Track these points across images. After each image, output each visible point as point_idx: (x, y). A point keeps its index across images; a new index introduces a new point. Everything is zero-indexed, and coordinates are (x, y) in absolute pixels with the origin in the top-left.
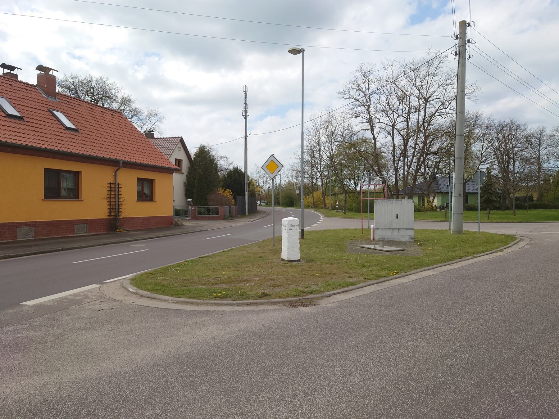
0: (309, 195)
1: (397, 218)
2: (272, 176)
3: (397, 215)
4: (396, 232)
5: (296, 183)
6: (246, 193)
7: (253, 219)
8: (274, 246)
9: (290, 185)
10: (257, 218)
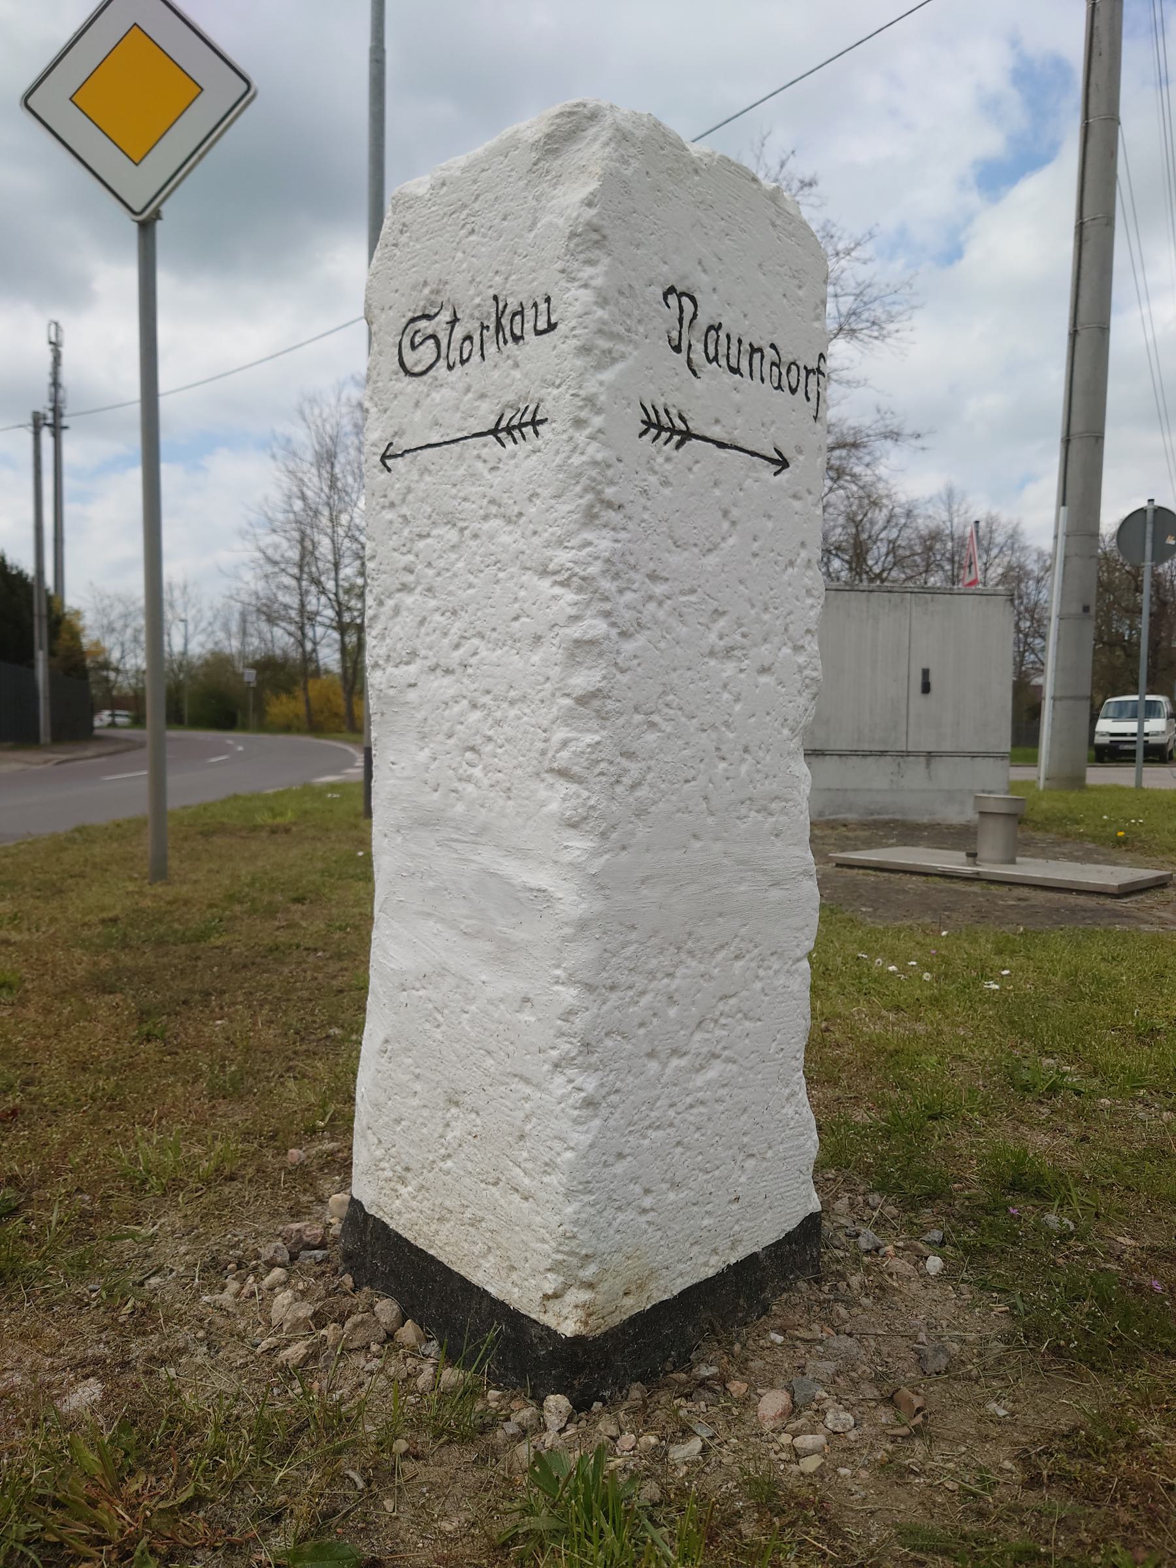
0: (289, 692)
1: (926, 688)
2: (140, 185)
3: (926, 673)
4: (915, 774)
5: (242, 654)
6: (41, 656)
7: (65, 757)
8: (160, 873)
9: (219, 663)
10: (88, 753)
